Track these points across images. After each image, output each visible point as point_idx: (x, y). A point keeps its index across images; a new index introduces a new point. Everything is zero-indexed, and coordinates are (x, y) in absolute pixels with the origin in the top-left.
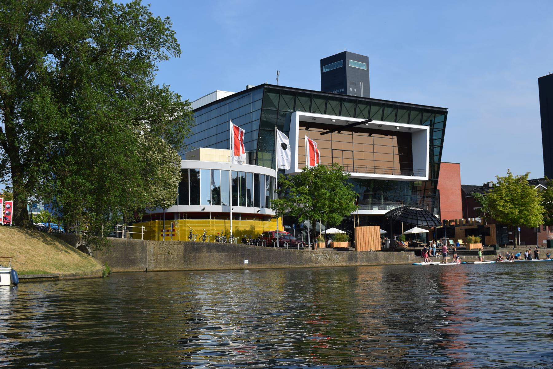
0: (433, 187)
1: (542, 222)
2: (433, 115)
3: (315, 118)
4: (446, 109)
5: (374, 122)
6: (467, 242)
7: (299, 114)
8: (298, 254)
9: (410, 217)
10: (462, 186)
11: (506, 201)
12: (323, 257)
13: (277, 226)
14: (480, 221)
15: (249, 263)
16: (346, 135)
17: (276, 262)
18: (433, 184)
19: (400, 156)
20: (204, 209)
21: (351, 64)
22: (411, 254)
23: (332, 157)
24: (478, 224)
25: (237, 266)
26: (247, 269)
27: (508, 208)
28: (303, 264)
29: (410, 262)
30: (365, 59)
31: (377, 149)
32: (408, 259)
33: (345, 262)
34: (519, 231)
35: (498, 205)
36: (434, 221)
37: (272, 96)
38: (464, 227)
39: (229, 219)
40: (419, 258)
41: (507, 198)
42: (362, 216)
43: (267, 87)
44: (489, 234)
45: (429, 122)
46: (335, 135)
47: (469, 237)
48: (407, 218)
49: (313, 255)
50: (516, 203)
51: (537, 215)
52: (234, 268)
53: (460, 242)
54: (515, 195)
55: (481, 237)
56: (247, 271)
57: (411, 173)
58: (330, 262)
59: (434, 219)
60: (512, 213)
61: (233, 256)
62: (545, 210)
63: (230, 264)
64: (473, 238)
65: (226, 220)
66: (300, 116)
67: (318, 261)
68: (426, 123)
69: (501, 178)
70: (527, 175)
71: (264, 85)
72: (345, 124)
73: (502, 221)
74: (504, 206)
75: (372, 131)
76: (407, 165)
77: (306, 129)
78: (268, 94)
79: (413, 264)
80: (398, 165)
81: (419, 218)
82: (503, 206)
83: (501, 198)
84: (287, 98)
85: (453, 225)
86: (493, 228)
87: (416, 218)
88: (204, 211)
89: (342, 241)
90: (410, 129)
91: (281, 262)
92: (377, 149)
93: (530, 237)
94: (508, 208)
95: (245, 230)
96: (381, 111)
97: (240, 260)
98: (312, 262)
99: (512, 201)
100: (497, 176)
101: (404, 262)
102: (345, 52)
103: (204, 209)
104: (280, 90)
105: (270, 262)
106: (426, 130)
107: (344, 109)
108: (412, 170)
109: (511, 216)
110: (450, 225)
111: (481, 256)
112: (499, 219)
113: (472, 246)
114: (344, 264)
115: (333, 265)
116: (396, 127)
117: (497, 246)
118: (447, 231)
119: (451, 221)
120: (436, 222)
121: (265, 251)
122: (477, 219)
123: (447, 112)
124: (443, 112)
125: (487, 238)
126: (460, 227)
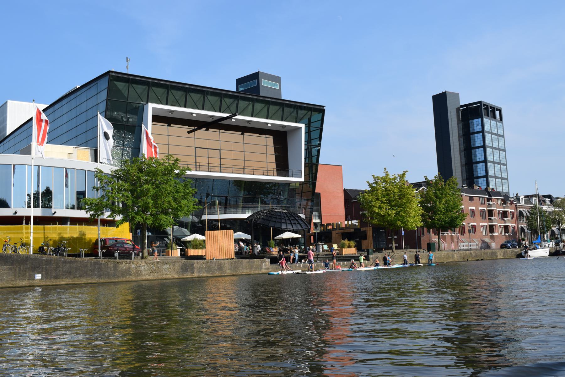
0: (311, 190)
1: (420, 224)
2: (310, 112)
3: (172, 112)
4: (323, 106)
5: (238, 117)
6: (341, 246)
7: (151, 106)
8: (112, 266)
9: (274, 219)
10: (345, 190)
11: (382, 202)
12: (147, 268)
13: (123, 232)
14: (357, 224)
15: (42, 279)
16: (213, 133)
17: (80, 276)
18: (311, 186)
19: (275, 156)
20: (16, 213)
21: (264, 83)
22: (265, 262)
23: (196, 156)
25: (24, 283)
26: (38, 286)
27: (384, 210)
28: (118, 277)
29: (263, 271)
30: (277, 79)
31: (248, 148)
32: (261, 268)
33: (177, 272)
34: (403, 234)
35: (374, 206)
36: (300, 224)
37: (121, 85)
38: (340, 231)
40: (275, 266)
41: (384, 199)
42: (223, 221)
43: (113, 74)
44: (365, 238)
45: (306, 120)
46: (201, 133)
47: (343, 241)
49: (133, 266)
50: (393, 204)
51: (415, 218)
52: (21, 285)
53: (335, 246)
54: (392, 195)
55: (356, 241)
56: (39, 289)
57: (287, 175)
58: (156, 274)
59: (300, 222)
60: (389, 215)
61: (20, 270)
62: (423, 211)
63: (15, 280)
64: (347, 242)
65: (46, 226)
66: (154, 109)
67: (139, 274)
68: (302, 121)
69: (378, 177)
70: (404, 174)
71: (109, 72)
72: (210, 120)
74: (382, 209)
75: (244, 129)
76: (283, 166)
77: (168, 126)
78: (115, 82)
79: (269, 274)
80: (274, 166)
81: (283, 221)
82: (380, 208)
83: (378, 199)
84: (140, 88)
86: (369, 232)
87: (279, 220)
88: (17, 215)
89: (199, 249)
90: (283, 126)
91: (88, 276)
92: (248, 148)
93: (412, 240)
94: (384, 210)
95: (72, 237)
96: (251, 107)
97: (30, 275)
98: (130, 275)
99: (389, 202)
101: (257, 272)
102: (258, 73)
103: (16, 213)
104: (129, 79)
105: (72, 276)
106: (301, 128)
107: (207, 103)
108: (288, 171)
109: (389, 218)
111: (362, 261)
112: (375, 222)
113: (346, 251)
114: (176, 276)
115: (160, 277)
116: (267, 124)
118: (325, 236)
119: (328, 225)
120: (303, 225)
121: (65, 262)
122: (353, 222)
123: (324, 110)
124: (320, 110)
125: (363, 242)
126: (337, 231)
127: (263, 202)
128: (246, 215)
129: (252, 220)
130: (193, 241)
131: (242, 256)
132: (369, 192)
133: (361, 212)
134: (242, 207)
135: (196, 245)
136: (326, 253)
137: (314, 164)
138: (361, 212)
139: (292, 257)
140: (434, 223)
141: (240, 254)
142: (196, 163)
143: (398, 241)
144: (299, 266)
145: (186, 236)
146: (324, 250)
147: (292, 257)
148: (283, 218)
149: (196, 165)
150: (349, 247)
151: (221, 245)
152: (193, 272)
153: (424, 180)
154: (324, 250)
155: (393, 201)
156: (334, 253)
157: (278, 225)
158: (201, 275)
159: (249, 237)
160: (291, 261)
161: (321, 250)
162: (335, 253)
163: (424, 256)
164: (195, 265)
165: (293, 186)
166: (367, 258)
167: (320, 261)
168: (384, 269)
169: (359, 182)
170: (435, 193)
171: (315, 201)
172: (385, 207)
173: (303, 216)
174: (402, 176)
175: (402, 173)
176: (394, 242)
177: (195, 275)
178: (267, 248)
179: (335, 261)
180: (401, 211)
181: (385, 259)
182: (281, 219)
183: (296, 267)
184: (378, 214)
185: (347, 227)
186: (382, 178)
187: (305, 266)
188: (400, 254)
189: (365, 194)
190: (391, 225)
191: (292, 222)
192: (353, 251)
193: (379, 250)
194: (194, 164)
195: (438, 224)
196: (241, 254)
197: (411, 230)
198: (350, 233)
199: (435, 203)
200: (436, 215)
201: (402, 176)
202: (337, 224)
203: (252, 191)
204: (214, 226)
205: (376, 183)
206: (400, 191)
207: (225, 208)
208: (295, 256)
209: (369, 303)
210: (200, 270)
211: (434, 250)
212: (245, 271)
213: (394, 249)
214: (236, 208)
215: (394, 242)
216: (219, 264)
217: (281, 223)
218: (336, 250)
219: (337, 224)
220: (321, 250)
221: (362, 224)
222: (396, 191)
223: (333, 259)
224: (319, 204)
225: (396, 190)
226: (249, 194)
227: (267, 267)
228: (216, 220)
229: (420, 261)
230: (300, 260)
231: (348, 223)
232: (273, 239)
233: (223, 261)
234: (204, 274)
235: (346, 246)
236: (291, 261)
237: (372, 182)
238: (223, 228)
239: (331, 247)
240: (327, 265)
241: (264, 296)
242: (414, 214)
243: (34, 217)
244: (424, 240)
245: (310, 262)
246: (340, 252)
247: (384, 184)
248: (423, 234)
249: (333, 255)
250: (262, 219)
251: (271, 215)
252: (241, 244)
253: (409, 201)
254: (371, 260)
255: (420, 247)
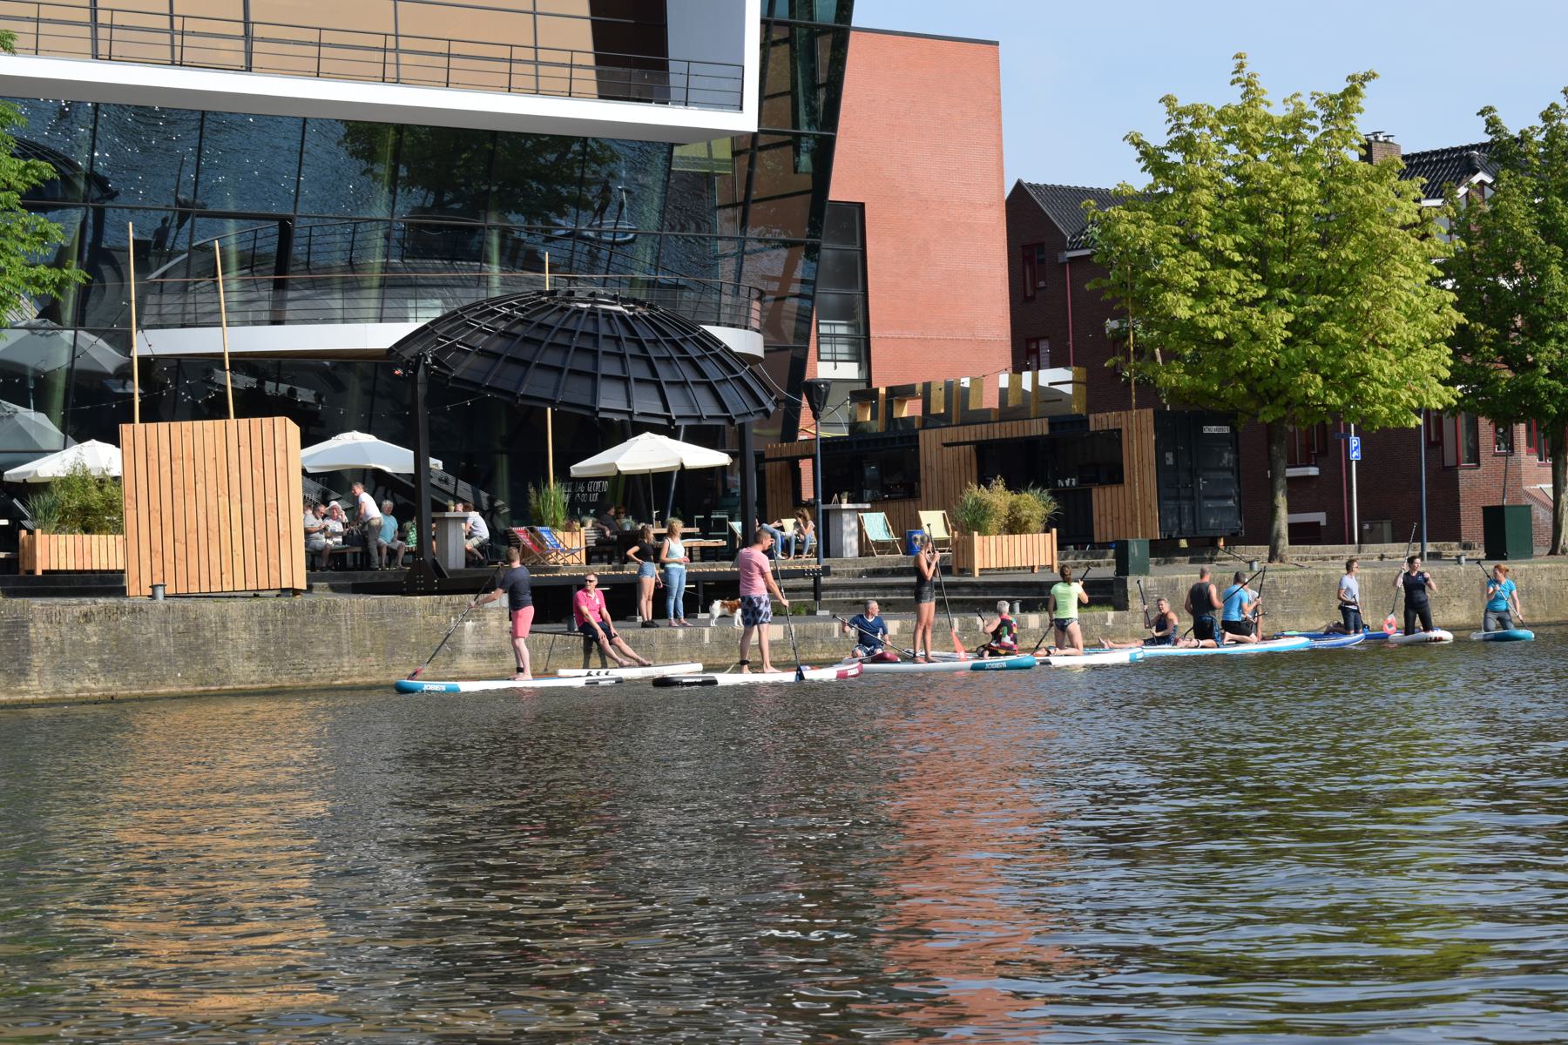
0: (806, 182)
6: (969, 522)
9: (553, 358)
11: (1218, 259)
24: (1058, 410)
27: (1224, 304)
34: (1355, 455)
35: (1168, 286)
39: (132, 421)
41: (1226, 242)
42: (244, 362)
44: (1115, 476)
47: (975, 493)
48: (526, 364)
51: (1408, 358)
53: (933, 522)
54: (1277, 221)
55: (1056, 494)
57: (658, 94)
59: (713, 372)
60: (1255, 337)
62: (1460, 318)
64: (999, 497)
69: (1194, 111)
70: (1352, 92)
73: (1197, 393)
80: (581, 36)
81: (608, 367)
82: (1202, 293)
83: (1190, 242)
85: (909, 421)
86: (1139, 436)
87: (584, 363)
93: (1408, 490)
99: (1260, 256)
100: (1168, 100)
108: (663, 66)
110: (890, 420)
112: (1174, 377)
113: (993, 553)
117: (1136, 550)
118: (880, 462)
119: (899, 393)
120: (729, 393)
122: (1047, 376)
125: (1103, 499)
126: (950, 434)
127: (519, 257)
128: (381, 335)
129: (419, 358)
130: (66, 483)
131: (365, 577)
132: (1149, 199)
133: (1112, 324)
134: (384, 285)
135: (85, 510)
136: (874, 562)
137: (825, 30)
138: (1112, 324)
139: (649, 583)
140: (1530, 391)
141: (345, 566)
142: (246, 22)
143: (1325, 493)
144: (688, 641)
145: (43, 453)
146: (865, 547)
147: (649, 583)
148: (605, 346)
149: (94, 23)
150: (1015, 526)
151: (218, 510)
152: (23, 673)
153: (1475, 134)
154: (865, 547)
155: (1287, 255)
156: (924, 557)
157: (575, 392)
158: (71, 689)
159: (396, 459)
160: (646, 606)
161: (851, 543)
162: (929, 562)
163: (1458, 583)
164: (38, 631)
165: (695, 161)
166: (1104, 594)
167: (835, 607)
168: (1197, 659)
169: (1086, 148)
170: (1544, 209)
171: (828, 251)
172: (1232, 287)
173: (742, 341)
174: (1342, 105)
175: (1339, 87)
176: (1281, 501)
177: (37, 687)
178: (520, 531)
179: (928, 607)
180: (1328, 314)
181: (1199, 601)
182: (594, 354)
183: (670, 642)
184: (1190, 330)
185: (1009, 410)
186: (1222, 117)
187: (723, 643)
188: (1319, 570)
189: (1113, 211)
190: (1271, 397)
191: (664, 374)
192: (1034, 551)
193: (1188, 538)
194: (239, 29)
195: (1552, 394)
196: (365, 561)
197: (1384, 430)
198: (1030, 443)
199: (1537, 266)
200: (1543, 340)
201: (1342, 105)
202: (949, 387)
203: (461, 184)
204: (184, 391)
205: (1186, 144)
206: (1328, 195)
207: (280, 286)
208: (665, 576)
209: (561, 909)
210: (65, 660)
211: (1526, 552)
212: (353, 669)
213: (1284, 542)
214: (340, 284)
215: (1281, 501)
216: (192, 621)
217: (593, 377)
218: (940, 543)
219: (949, 387)
220: (851, 543)
221: (1103, 388)
222: (1300, 193)
223: (919, 597)
224: (854, 272)
225: (1304, 191)
226: (440, 205)
227: (489, 643)
228: (215, 359)
229: (1436, 617)
230: (696, 602)
231: (1015, 383)
232: (563, 473)
233: (210, 606)
234: (95, 686)
235: (993, 523)
236: (646, 606)
237: (1158, 136)
238: (253, 405)
239: (905, 528)
240: (867, 638)
241: (506, 822)
242: (1404, 332)
243: (231, 354)
244: (1477, 487)
245: (752, 616)
246: (957, 557)
247: (1232, 149)
248: (1475, 457)
249: (917, 571)
250: (484, 353)
251: (539, 332)
252: (368, 503)
253: (1379, 255)
254: (1135, 603)
255: (1446, 528)
